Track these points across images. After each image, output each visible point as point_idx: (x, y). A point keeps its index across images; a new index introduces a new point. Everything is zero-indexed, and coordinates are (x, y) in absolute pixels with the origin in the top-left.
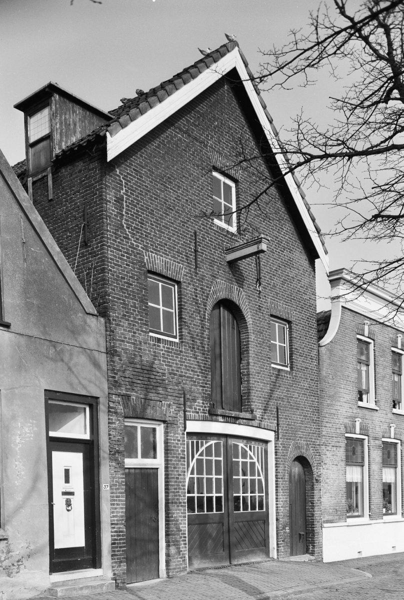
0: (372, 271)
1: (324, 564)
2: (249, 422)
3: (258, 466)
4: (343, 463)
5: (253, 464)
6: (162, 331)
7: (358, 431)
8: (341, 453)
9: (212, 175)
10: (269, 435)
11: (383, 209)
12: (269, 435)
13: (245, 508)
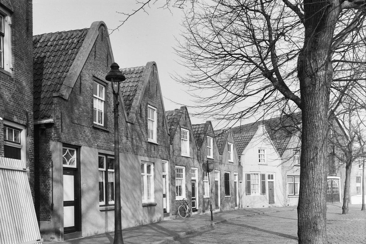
0: (246, 118)
1: (184, 165)
2: (336, 176)
3: (337, 184)
4: (355, 183)
5: (336, 184)
6: (7, 139)
7: (359, 175)
8: (355, 180)
9: (354, 43)
10: (339, 178)
11: (360, 34)
12: (339, 178)
13: (335, 192)
